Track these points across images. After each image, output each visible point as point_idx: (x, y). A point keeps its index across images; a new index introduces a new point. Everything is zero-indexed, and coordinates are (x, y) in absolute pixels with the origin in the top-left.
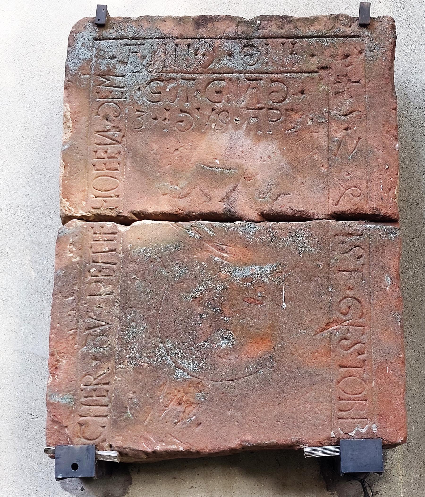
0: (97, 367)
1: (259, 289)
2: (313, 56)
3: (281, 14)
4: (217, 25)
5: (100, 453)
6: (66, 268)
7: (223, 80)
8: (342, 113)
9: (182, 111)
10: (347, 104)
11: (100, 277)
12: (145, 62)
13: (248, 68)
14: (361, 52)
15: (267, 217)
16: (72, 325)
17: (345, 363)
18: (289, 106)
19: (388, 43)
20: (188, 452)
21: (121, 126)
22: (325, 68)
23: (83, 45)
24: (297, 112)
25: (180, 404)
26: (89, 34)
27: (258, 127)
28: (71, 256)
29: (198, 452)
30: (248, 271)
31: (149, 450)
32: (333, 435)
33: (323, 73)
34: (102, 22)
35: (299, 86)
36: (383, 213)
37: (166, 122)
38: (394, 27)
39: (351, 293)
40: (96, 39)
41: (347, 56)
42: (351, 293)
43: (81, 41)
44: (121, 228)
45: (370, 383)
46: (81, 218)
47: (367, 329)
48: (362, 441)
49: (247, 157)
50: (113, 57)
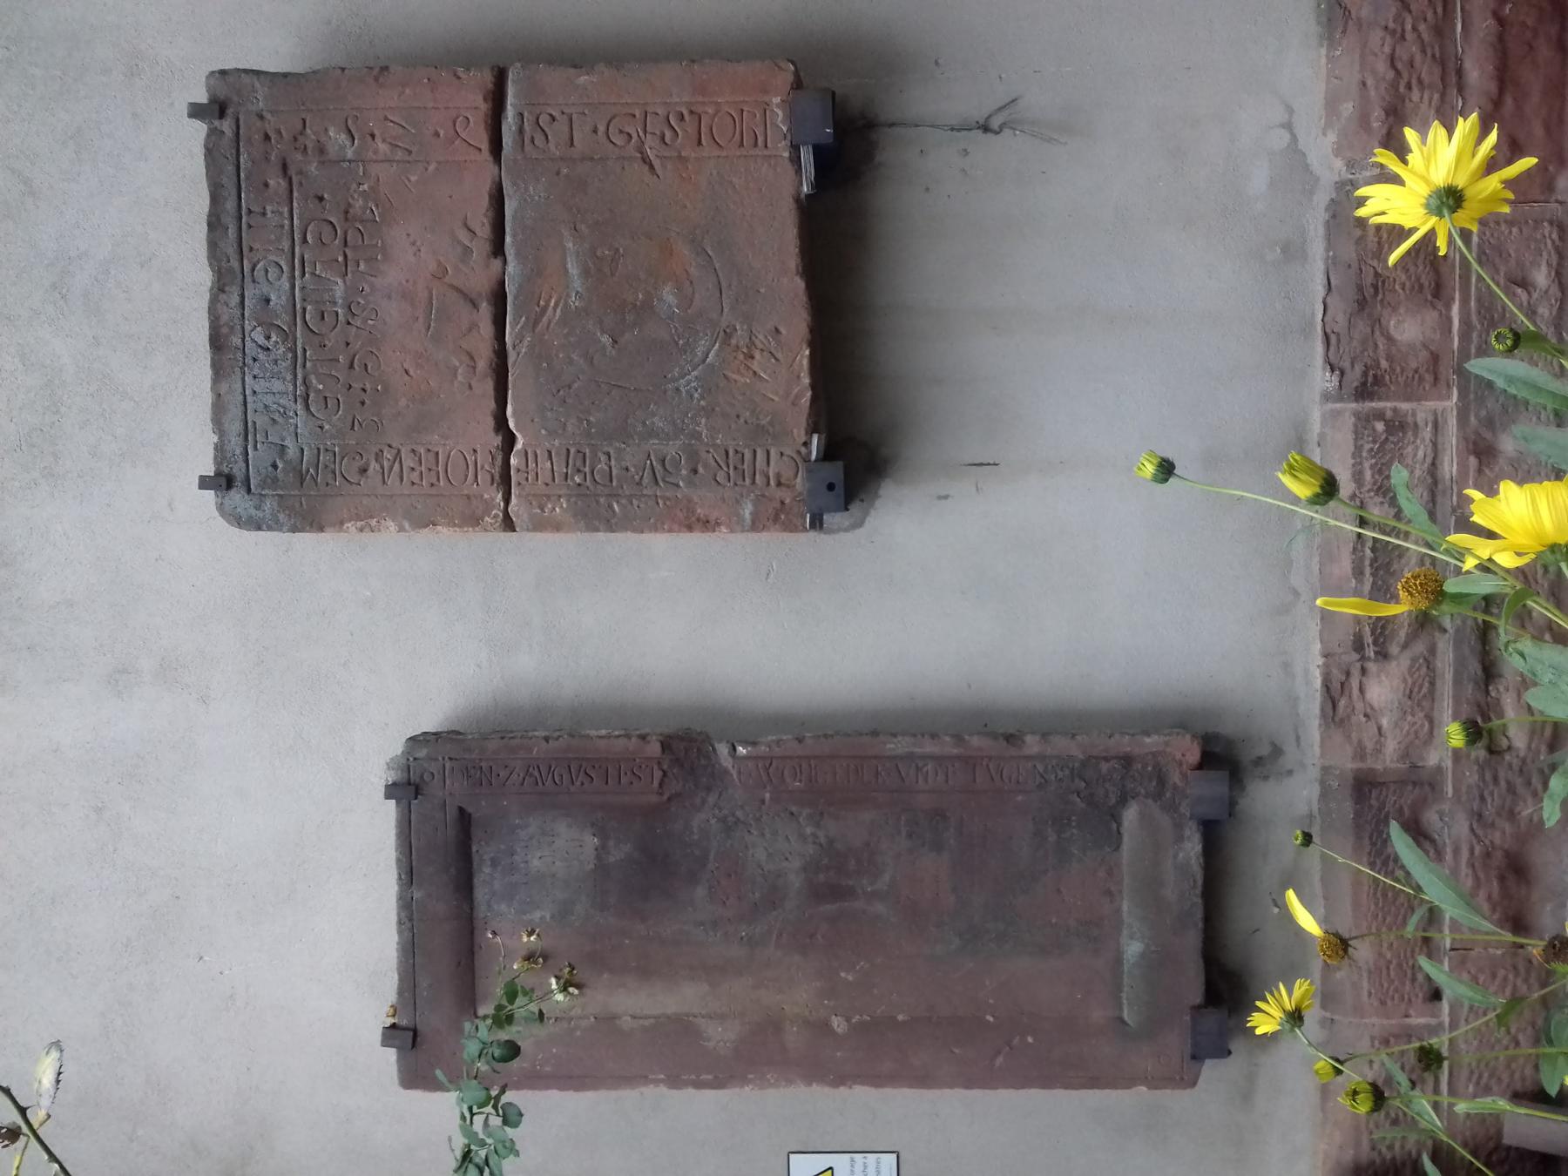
0: (706, 466)
1: (599, 253)
2: (266, 185)
3: (202, 230)
4: (225, 318)
5: (813, 457)
6: (575, 516)
7: (304, 310)
8: (348, 143)
9: (351, 366)
10: (337, 137)
11: (587, 469)
12: (280, 420)
13: (285, 276)
14: (261, 117)
15: (498, 249)
16: (651, 503)
17: (695, 136)
18: (342, 216)
19: (246, 79)
20: (812, 344)
21: (375, 449)
22: (285, 167)
23: (258, 508)
24: (349, 205)
25: (752, 357)
26: (236, 497)
27: (371, 260)
28: (559, 510)
29: (811, 331)
30: (573, 270)
31: (809, 394)
32: (786, 154)
33: (292, 172)
34: (221, 481)
35: (312, 204)
36: (491, 86)
37: (368, 387)
38: (223, 72)
39: (602, 129)
40: (249, 491)
41: (267, 137)
42: (602, 129)
43: (253, 512)
44: (519, 446)
45: (717, 103)
46: (507, 500)
47: (650, 110)
48: (793, 117)
49: (423, 251)
50: (275, 466)
